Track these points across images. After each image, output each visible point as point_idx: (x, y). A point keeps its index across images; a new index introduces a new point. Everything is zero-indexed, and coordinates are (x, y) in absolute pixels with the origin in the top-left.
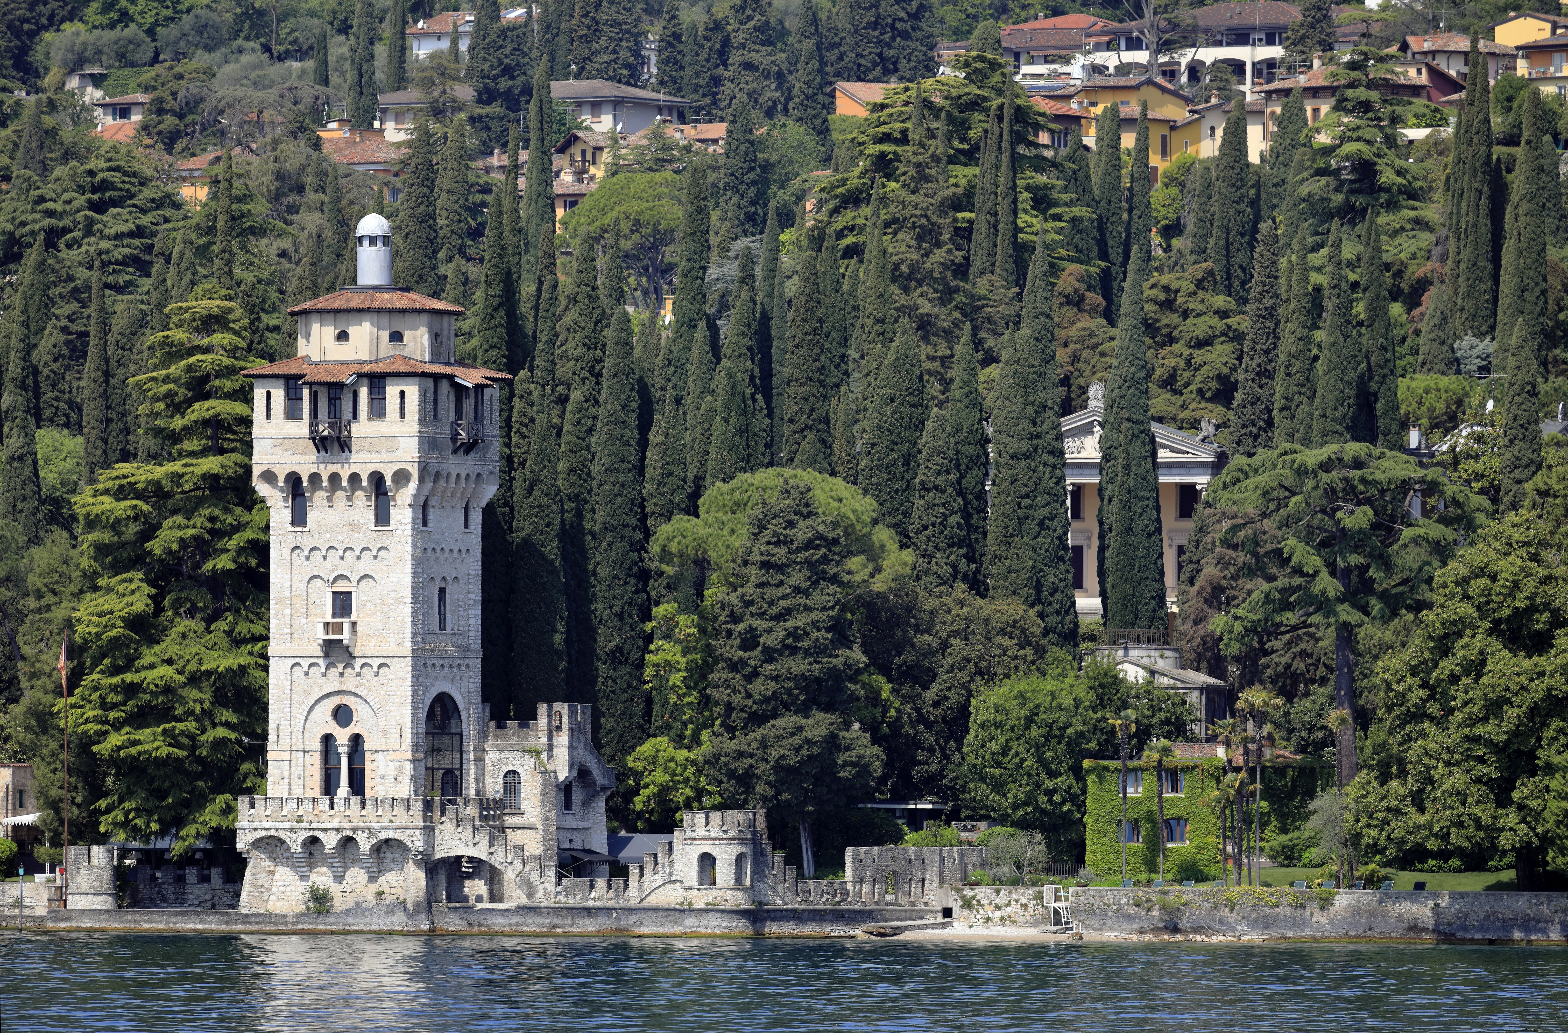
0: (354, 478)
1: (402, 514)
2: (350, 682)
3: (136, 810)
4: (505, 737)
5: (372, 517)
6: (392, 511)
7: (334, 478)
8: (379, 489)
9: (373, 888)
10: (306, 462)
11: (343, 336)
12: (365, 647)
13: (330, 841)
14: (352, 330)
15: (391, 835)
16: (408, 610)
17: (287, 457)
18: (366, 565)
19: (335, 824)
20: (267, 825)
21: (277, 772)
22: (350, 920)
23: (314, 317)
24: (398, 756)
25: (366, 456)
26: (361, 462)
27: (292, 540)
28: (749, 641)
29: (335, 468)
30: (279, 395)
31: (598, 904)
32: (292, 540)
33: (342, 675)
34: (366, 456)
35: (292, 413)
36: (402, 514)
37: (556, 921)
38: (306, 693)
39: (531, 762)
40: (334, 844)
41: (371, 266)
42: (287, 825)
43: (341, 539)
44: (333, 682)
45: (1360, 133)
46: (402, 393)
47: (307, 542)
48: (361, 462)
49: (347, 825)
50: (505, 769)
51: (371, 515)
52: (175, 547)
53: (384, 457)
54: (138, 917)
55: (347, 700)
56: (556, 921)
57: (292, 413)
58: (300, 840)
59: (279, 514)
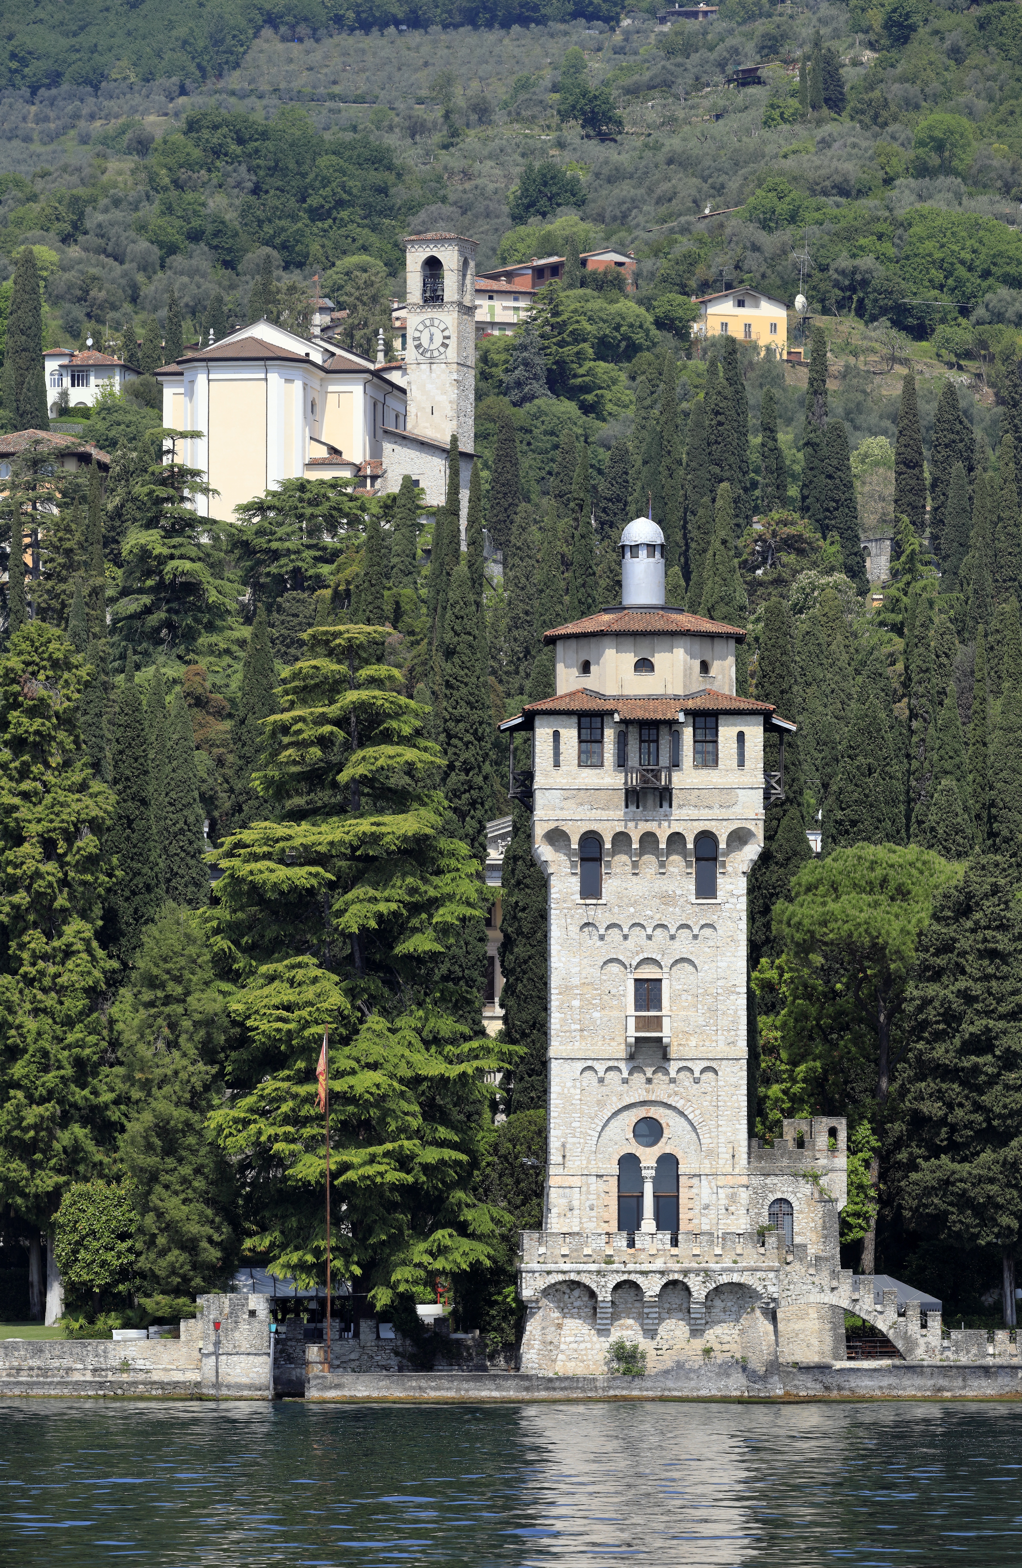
0: (676, 839)
2: (661, 1090)
3: (333, 1249)
4: (772, 1158)
5: (693, 888)
6: (720, 880)
7: (649, 839)
8: (706, 853)
9: (698, 1344)
10: (609, 820)
11: (644, 665)
14: (659, 659)
15: (736, 1278)
17: (583, 812)
18: (683, 946)
19: (658, 1265)
20: (566, 1267)
21: (563, 1202)
22: (670, 1384)
23: (607, 641)
24: (731, 1181)
25: (694, 813)
27: (581, 915)
28: (980, 1044)
29: (651, 827)
30: (570, 735)
31: (998, 1361)
32: (581, 915)
33: (649, 1081)
34: (694, 813)
35: (589, 755)
36: (733, 886)
37: (942, 1382)
38: (601, 1104)
39: (806, 1188)
40: (657, 1290)
41: (644, 581)
42: (593, 1267)
43: (650, 914)
44: (637, 1090)
45: (183, 550)
46: (741, 736)
47: (602, 918)
48: (685, 819)
49: (677, 1267)
50: (772, 1198)
51: (691, 885)
52: (373, 924)
53: (717, 813)
54: (423, 1383)
55: (655, 1112)
56: (942, 1382)
58: (611, 1285)
59: (564, 883)
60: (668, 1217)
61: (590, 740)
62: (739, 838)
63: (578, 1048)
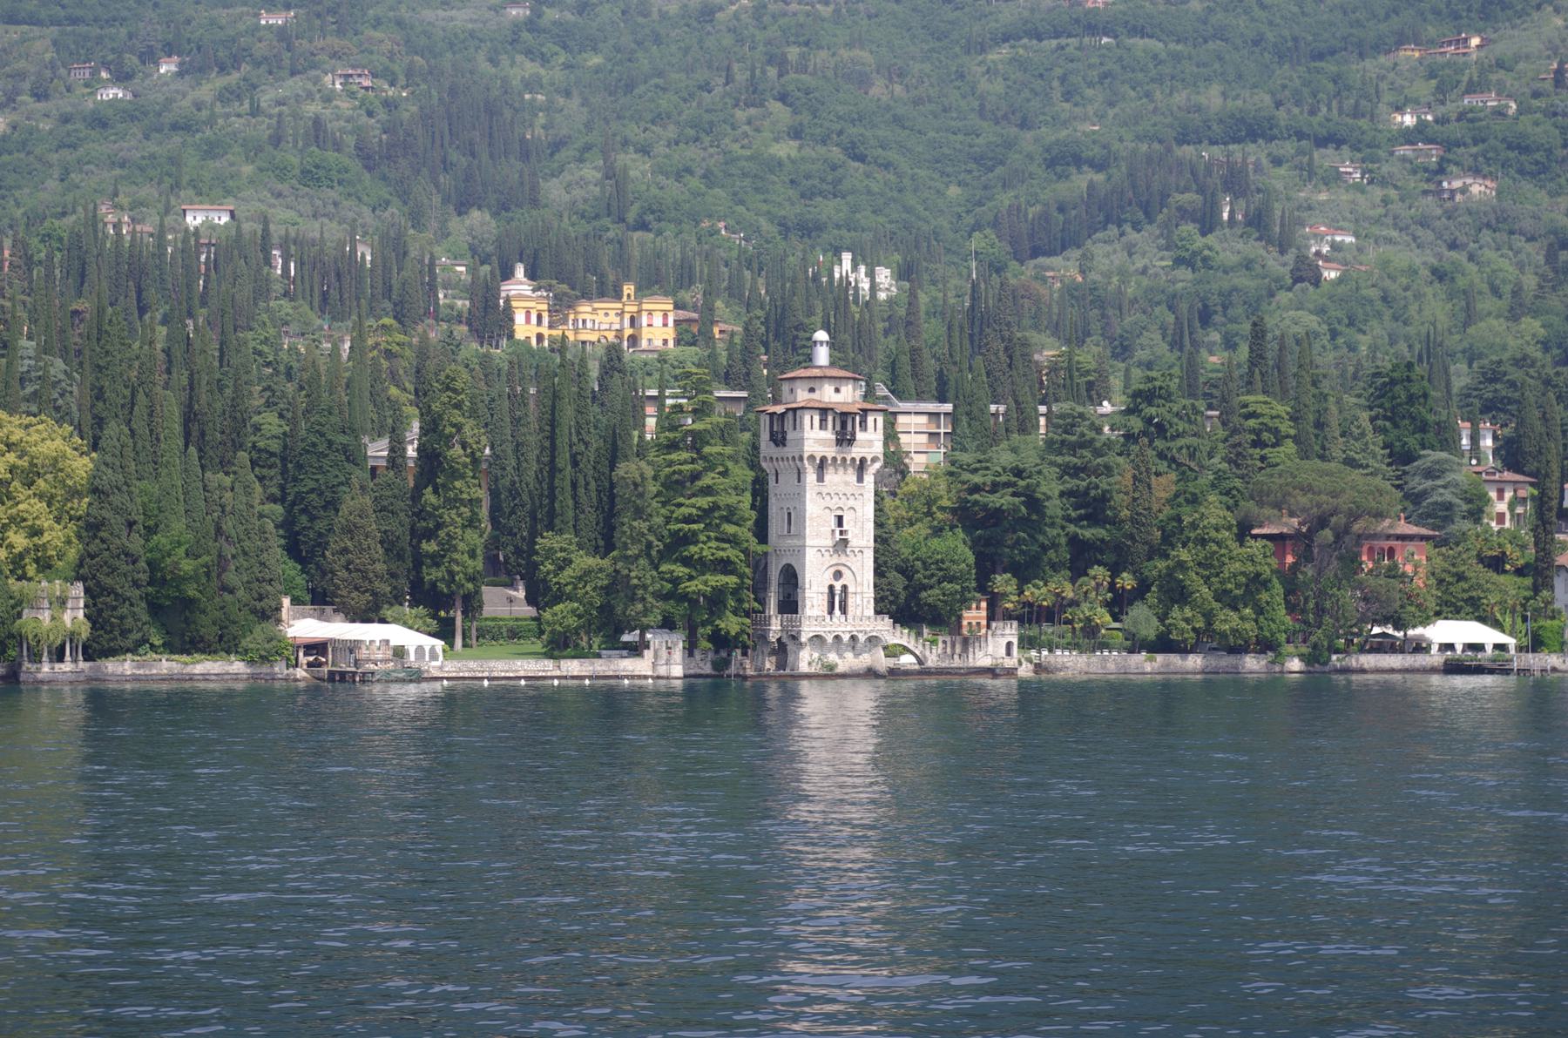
0: (853, 460)
1: (869, 479)
8: (861, 466)
10: (831, 452)
11: (837, 390)
12: (854, 542)
13: (846, 638)
14: (843, 389)
16: (808, 530)
18: (851, 503)
26: (856, 452)
30: (817, 418)
32: (817, 489)
35: (823, 426)
36: (869, 479)
41: (822, 356)
43: (842, 489)
44: (835, 560)
47: (825, 491)
48: (856, 452)
57: (823, 426)
60: (844, 610)
61: (823, 421)
62: (874, 460)
63: (816, 542)
